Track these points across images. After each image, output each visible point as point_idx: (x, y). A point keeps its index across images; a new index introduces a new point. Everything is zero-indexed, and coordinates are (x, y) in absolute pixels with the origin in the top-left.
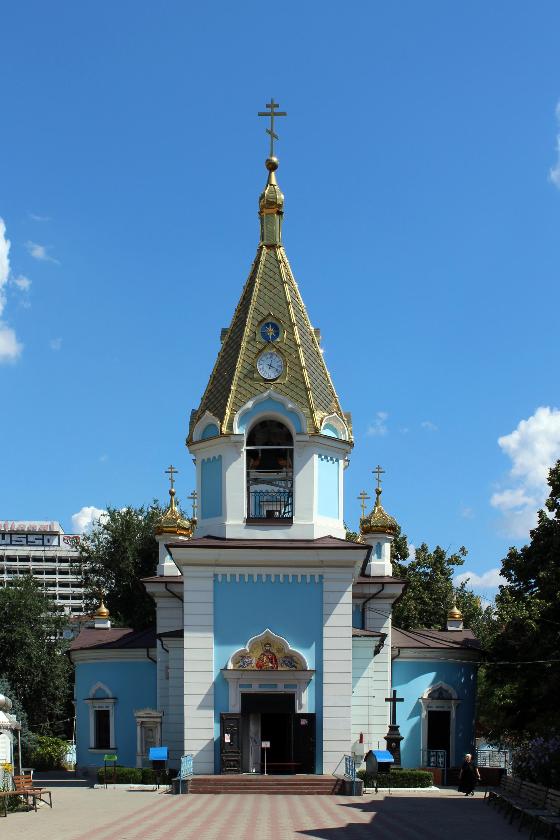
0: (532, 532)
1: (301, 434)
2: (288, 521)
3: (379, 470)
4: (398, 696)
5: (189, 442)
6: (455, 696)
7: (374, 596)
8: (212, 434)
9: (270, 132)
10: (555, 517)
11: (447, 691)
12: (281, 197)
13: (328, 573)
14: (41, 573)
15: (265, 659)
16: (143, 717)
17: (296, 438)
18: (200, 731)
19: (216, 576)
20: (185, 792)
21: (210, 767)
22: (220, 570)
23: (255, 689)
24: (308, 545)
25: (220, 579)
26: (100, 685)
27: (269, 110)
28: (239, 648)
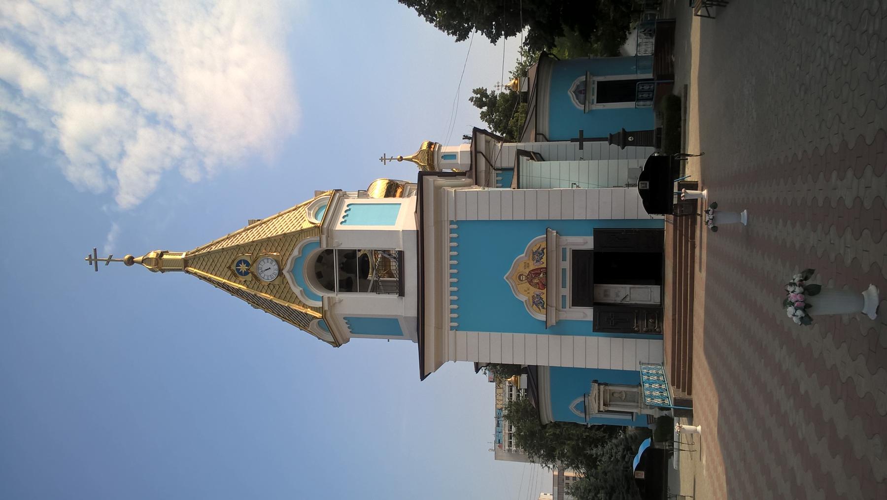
3: (383, 159)
4: (578, 136)
6: (583, 78)
7: (488, 161)
11: (578, 86)
13: (449, 215)
15: (536, 281)
16: (599, 403)
17: (324, 247)
19: (452, 328)
20: (690, 403)
21: (655, 344)
22: (447, 324)
23: (567, 292)
24: (421, 233)
25: (455, 324)
26: (572, 407)
27: (93, 262)
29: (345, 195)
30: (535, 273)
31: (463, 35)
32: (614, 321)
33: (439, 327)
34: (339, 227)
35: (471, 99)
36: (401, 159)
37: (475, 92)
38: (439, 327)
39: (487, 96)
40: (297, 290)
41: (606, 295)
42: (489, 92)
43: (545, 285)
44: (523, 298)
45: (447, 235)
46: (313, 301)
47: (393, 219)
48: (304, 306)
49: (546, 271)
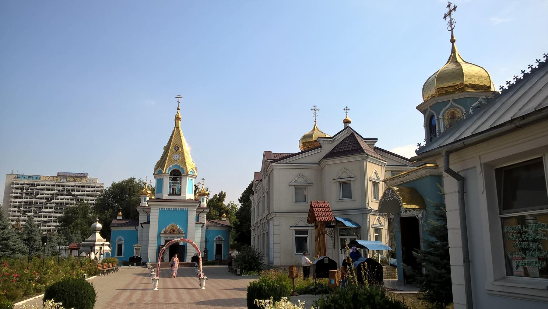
0: (256, 174)
2: (179, 194)
5: (154, 174)
12: (180, 117)
22: (161, 207)
24: (184, 201)
26: (120, 237)
28: (253, 280)
29: (195, 178)
30: (174, 231)
33: (160, 205)
35: (222, 192)
38: (160, 205)
39: (223, 198)
44: (167, 228)
45: (184, 208)
46: (167, 169)
48: (167, 168)
49: (174, 233)
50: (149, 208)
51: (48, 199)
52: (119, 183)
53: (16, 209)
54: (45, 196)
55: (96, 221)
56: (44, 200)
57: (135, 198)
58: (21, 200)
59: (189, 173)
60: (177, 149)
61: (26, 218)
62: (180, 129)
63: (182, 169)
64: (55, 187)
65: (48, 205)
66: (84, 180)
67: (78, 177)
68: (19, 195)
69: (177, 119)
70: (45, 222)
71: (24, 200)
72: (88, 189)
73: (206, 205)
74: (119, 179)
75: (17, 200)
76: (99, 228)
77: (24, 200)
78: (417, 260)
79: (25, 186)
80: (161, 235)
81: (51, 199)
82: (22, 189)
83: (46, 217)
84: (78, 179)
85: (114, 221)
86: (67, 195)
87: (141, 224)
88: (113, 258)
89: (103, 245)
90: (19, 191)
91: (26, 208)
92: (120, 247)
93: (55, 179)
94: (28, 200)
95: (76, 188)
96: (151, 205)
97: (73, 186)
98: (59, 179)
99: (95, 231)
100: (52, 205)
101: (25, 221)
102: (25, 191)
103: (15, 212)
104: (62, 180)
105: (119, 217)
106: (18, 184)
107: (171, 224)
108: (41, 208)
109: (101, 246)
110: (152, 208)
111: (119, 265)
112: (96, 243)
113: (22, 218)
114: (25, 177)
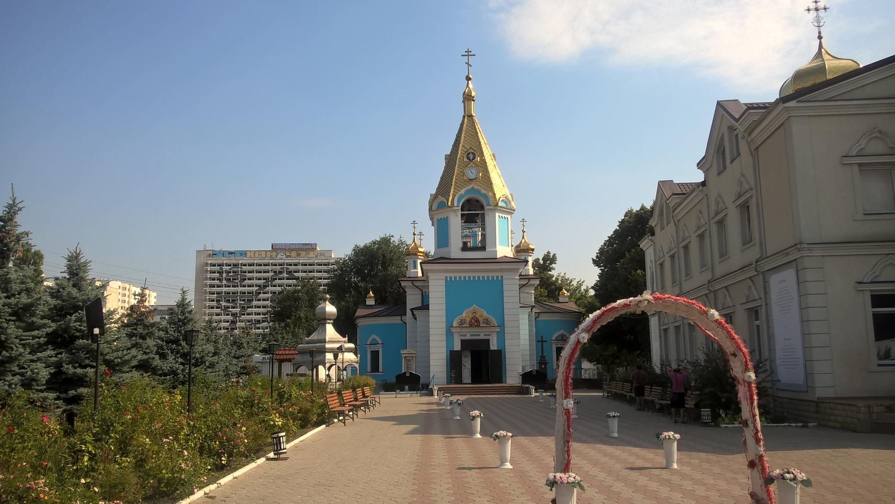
1: (489, 205)
2: (483, 248)
3: (523, 220)
8: (443, 206)
9: (468, 64)
10: (592, 288)
12: (473, 94)
14: (291, 265)
17: (486, 207)
18: (437, 366)
22: (449, 275)
23: (468, 337)
24: (494, 261)
26: (374, 336)
30: (477, 321)
31: (596, 263)
32: (454, 360)
33: (447, 271)
34: (497, 214)
35: (549, 252)
36: (524, 232)
37: (554, 255)
38: (447, 271)
40: (463, 192)
41: (466, 356)
42: (553, 265)
43: (471, 325)
44: (464, 314)
46: (456, 198)
47: (501, 244)
48: (454, 196)
49: (478, 326)
50: (425, 280)
51: (260, 286)
52: (365, 246)
53: (214, 304)
54: (255, 282)
55: (325, 300)
56: (255, 289)
57: (392, 270)
58: (219, 289)
59: (501, 204)
60: (471, 156)
61: (230, 318)
62: (476, 119)
63: (485, 196)
64: (270, 268)
65: (262, 296)
66: (311, 254)
67: (302, 250)
68: (217, 282)
69: (468, 98)
70: (258, 322)
71: (224, 289)
72: (259, 268)
73: (531, 272)
74: (366, 237)
75: (216, 289)
76: (331, 314)
77: (224, 289)
78: (52, 371)
79: (225, 268)
80: (453, 330)
81: (265, 286)
82: (220, 273)
83: (259, 314)
84: (303, 253)
85: (360, 312)
86: (287, 279)
87: (412, 310)
88: (364, 377)
89: (340, 349)
90: (217, 275)
91: (228, 301)
92: (375, 354)
93: (269, 254)
94: (232, 289)
95: (300, 267)
96: (428, 271)
97: (295, 265)
98: (274, 254)
99: (323, 320)
100: (266, 296)
101: (228, 322)
102: (224, 275)
103: (213, 308)
104: (279, 256)
105: (370, 302)
106: (214, 265)
107: (472, 308)
108: (250, 301)
109: (338, 354)
110: (431, 276)
111: (376, 391)
112: (328, 346)
113: (223, 317)
114: (223, 253)
